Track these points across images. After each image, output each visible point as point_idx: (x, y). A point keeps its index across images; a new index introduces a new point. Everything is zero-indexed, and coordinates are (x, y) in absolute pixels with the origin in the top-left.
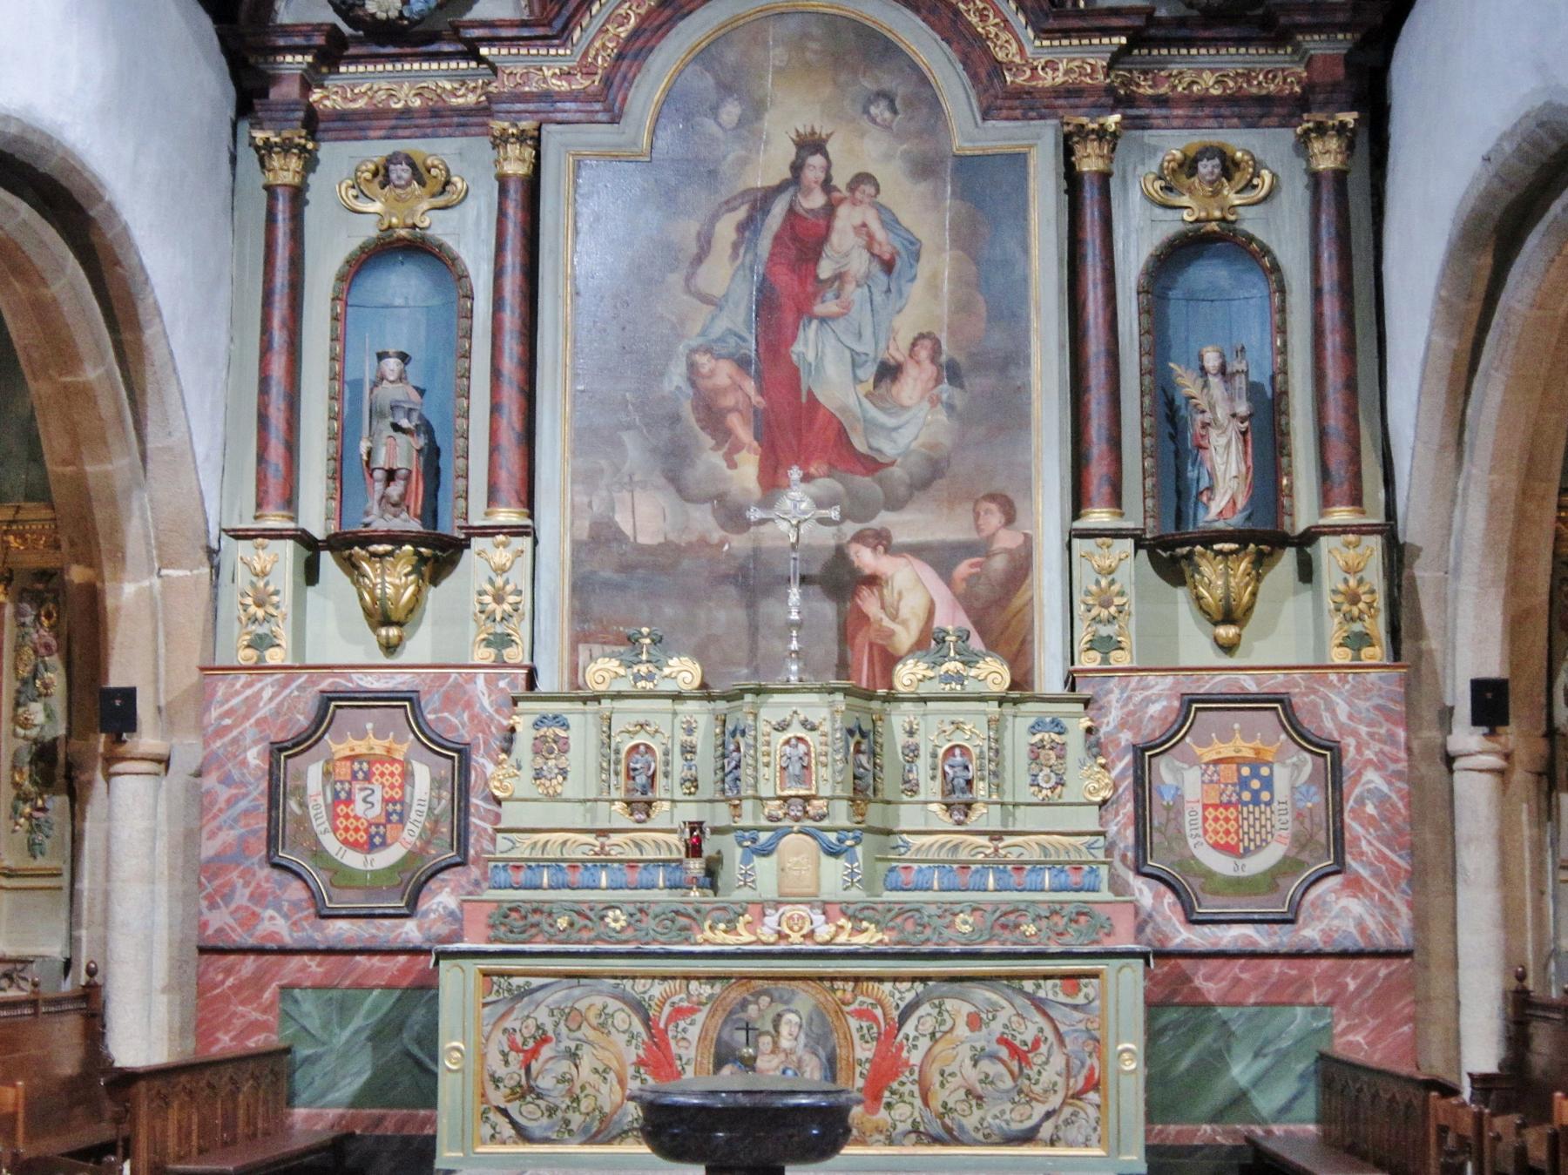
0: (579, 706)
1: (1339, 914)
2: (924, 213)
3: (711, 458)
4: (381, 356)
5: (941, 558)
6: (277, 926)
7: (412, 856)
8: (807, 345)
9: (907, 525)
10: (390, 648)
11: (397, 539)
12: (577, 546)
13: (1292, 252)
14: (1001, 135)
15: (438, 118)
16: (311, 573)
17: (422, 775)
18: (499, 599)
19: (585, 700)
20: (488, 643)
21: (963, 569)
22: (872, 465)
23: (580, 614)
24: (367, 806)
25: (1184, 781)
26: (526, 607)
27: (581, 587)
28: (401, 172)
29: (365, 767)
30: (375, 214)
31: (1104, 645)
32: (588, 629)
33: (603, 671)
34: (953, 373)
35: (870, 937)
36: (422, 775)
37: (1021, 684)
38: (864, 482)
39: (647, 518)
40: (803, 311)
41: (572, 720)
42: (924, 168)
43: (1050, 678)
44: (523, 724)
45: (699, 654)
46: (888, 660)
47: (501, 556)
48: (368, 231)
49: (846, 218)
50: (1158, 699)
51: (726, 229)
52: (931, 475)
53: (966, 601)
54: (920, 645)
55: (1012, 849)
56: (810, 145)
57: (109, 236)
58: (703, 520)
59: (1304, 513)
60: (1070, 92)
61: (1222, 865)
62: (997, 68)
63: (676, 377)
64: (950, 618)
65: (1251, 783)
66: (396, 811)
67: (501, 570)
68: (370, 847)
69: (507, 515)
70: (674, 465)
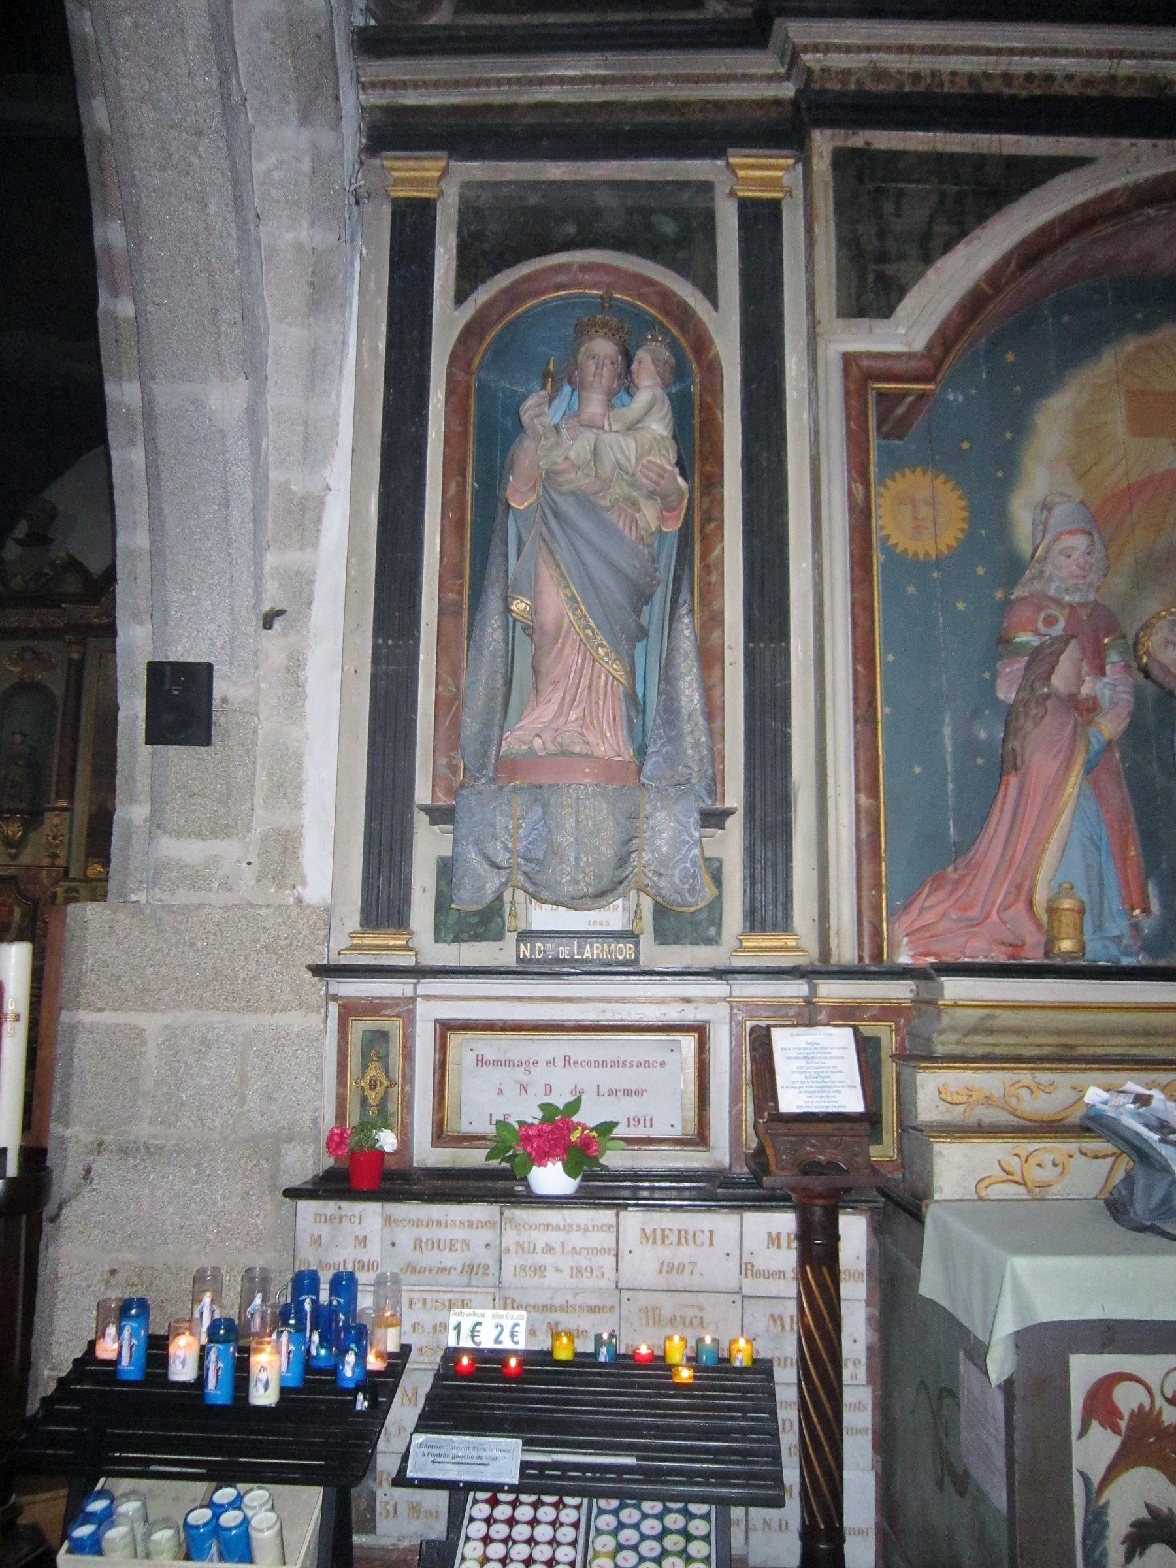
0: (84, 884)
4: (14, 734)
10: (14, 857)
11: (13, 812)
12: (91, 817)
17: (17, 912)
18: (55, 838)
19: (86, 881)
20: (49, 857)
26: (66, 841)
28: (28, 655)
36: (17, 912)
41: (81, 890)
44: (59, 890)
47: (56, 820)
57: (65, 1017)
67: (56, 826)
69: (62, 803)
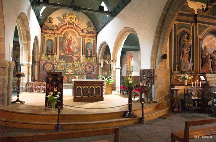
1: (94, 73)
2: (76, 41)
3: (66, 51)
5: (76, 57)
6: (44, 73)
7: (51, 70)
8: (70, 46)
9: (75, 55)
13: (93, 44)
14: (80, 37)
15: (52, 33)
16: (45, 55)
21: (77, 57)
22: (73, 52)
23: (59, 58)
24: (48, 67)
25: (87, 67)
27: (59, 57)
28: (50, 36)
29: (48, 65)
30: (48, 38)
31: (84, 61)
32: (59, 59)
33: (61, 61)
34: (77, 48)
35: (74, 74)
37: (80, 62)
38: (73, 53)
39: (62, 54)
40: (70, 45)
42: (76, 39)
43: (81, 62)
45: (129, 83)
46: (74, 61)
48: (48, 39)
49: (72, 40)
50: (86, 63)
51: (67, 40)
52: (76, 53)
53: (77, 59)
54: (75, 61)
55: (79, 70)
56: (71, 37)
58: (65, 54)
59: (92, 56)
60: (83, 35)
61: (89, 71)
62: (80, 34)
63: (64, 47)
64: (77, 60)
65: (90, 68)
66: (50, 68)
68: (49, 69)
70: (64, 52)
